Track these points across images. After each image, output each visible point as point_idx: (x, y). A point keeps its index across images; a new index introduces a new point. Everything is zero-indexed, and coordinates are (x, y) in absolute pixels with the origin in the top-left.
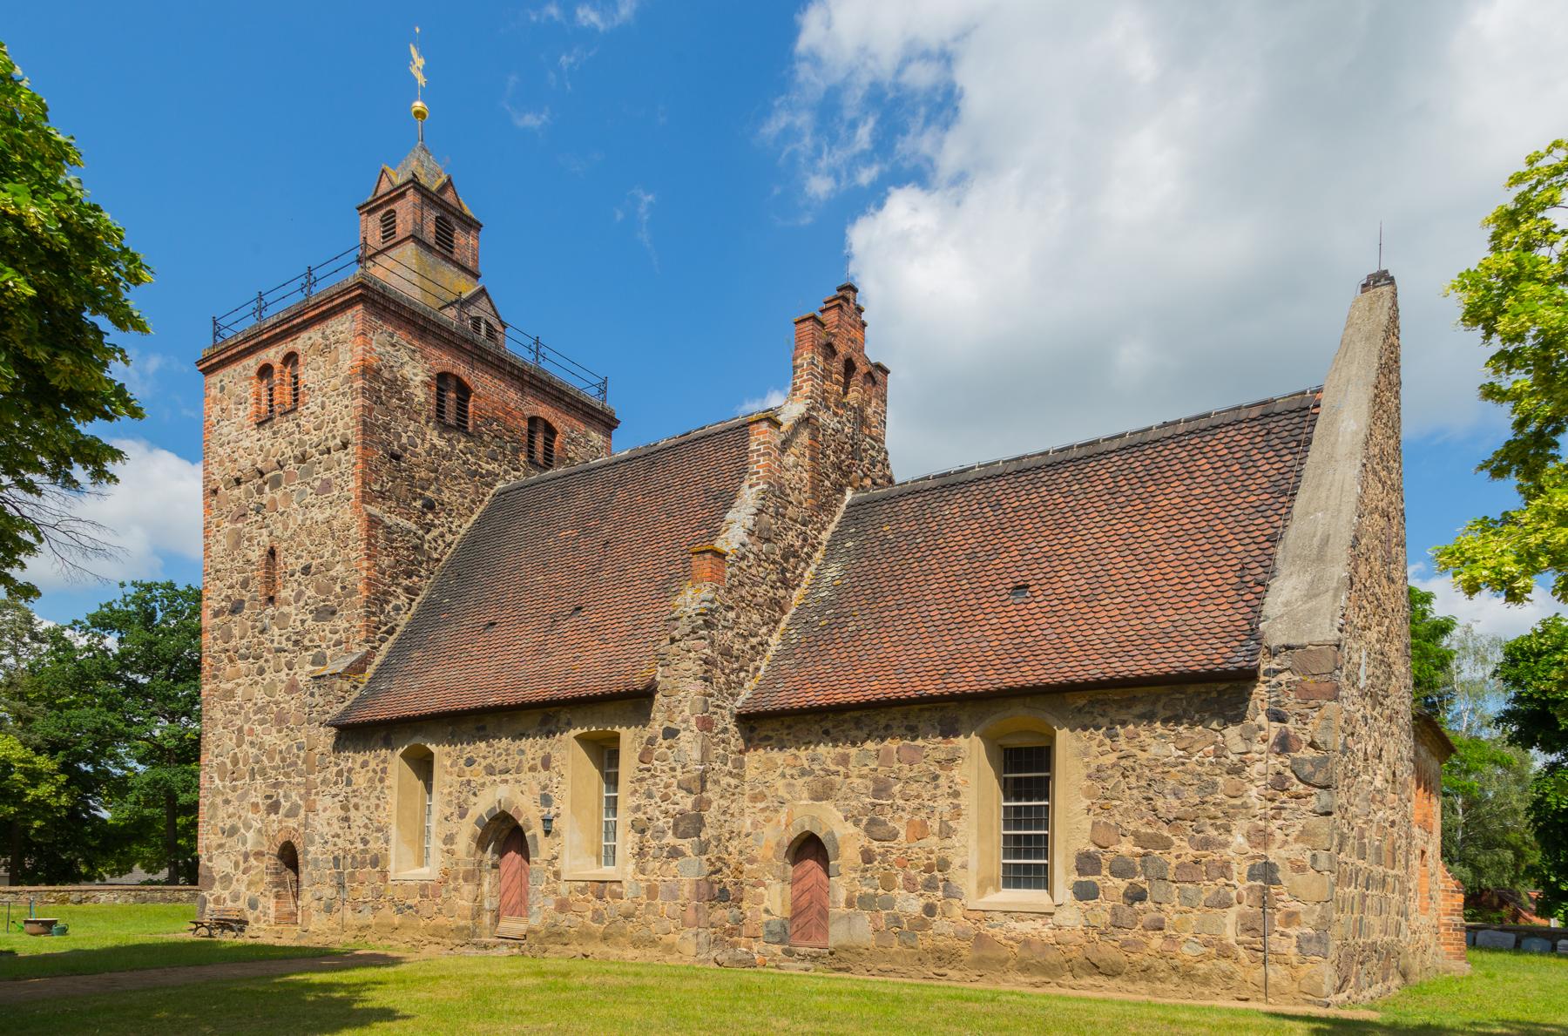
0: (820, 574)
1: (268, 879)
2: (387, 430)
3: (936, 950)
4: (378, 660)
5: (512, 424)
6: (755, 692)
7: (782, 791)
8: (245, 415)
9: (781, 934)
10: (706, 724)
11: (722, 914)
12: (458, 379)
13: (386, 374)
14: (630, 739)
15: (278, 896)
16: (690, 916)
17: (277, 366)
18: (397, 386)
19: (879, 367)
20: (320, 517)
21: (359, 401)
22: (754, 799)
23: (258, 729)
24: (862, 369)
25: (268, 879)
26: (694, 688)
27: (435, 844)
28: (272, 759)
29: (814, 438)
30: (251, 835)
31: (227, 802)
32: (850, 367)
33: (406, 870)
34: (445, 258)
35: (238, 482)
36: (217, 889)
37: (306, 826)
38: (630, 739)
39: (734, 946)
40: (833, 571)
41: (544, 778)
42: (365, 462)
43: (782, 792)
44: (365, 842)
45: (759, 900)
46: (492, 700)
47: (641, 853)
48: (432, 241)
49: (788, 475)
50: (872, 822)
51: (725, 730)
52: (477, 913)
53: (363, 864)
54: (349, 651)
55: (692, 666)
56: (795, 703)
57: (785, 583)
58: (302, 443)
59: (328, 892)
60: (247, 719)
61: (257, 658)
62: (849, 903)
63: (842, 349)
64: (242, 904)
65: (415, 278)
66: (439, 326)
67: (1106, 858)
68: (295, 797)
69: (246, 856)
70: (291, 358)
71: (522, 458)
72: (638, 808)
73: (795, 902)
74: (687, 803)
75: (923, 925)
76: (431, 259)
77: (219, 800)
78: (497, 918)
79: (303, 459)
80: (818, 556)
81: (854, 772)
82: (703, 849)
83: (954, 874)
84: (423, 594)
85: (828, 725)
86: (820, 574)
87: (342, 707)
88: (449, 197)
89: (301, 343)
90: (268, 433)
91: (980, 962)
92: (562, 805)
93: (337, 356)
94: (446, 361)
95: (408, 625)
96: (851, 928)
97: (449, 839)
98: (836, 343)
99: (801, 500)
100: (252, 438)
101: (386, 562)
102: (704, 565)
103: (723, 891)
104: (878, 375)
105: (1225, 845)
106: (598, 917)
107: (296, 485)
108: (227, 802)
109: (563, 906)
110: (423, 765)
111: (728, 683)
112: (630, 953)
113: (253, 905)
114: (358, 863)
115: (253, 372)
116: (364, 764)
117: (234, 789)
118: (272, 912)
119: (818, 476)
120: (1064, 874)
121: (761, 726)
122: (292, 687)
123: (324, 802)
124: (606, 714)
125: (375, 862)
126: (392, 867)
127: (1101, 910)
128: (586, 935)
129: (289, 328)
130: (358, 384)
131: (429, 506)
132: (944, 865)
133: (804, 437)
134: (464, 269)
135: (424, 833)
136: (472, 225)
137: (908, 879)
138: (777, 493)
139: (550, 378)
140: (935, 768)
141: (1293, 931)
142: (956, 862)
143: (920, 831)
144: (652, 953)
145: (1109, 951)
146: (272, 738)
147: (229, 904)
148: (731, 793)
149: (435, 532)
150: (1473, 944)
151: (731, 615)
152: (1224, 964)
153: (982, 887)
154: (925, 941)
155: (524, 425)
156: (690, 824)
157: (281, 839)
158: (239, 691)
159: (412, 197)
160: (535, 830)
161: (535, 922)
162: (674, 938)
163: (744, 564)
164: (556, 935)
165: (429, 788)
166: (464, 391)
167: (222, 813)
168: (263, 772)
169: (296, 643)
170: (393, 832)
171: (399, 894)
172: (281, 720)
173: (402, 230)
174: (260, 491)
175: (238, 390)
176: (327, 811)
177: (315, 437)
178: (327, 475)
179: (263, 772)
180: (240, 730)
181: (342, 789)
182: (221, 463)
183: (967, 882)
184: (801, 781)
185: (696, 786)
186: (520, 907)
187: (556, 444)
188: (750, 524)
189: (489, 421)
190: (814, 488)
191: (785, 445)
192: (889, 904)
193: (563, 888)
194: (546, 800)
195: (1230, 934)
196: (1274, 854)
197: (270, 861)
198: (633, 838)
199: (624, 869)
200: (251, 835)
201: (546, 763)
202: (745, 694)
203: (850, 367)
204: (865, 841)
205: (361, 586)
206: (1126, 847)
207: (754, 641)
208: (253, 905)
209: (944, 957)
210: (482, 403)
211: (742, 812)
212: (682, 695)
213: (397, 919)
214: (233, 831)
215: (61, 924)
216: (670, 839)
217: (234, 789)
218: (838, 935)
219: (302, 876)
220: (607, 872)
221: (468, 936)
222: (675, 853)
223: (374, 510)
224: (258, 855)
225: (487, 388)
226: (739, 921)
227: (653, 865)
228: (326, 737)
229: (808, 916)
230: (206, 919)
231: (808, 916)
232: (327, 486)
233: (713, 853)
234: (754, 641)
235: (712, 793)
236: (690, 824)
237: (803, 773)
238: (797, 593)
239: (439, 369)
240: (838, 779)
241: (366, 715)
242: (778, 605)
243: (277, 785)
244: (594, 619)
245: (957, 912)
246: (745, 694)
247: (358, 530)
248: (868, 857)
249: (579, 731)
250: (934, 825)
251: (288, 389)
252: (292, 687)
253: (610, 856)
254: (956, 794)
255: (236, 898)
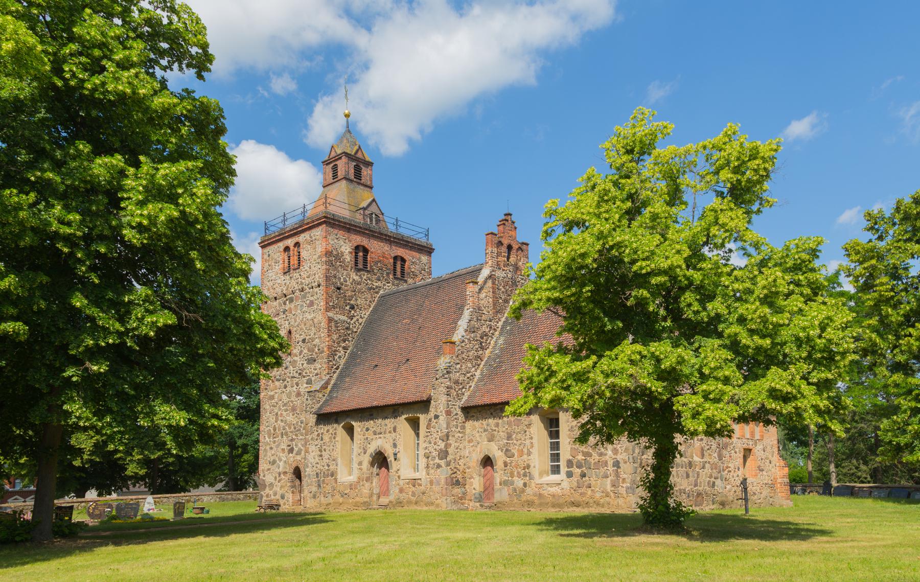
0: (497, 342)
1: (289, 484)
2: (335, 277)
3: (528, 501)
4: (332, 382)
5: (386, 261)
6: (469, 397)
7: (478, 438)
8: (278, 268)
9: (480, 499)
10: (448, 413)
11: (458, 491)
12: (364, 247)
13: (335, 253)
14: (423, 418)
15: (293, 492)
16: (444, 491)
17: (292, 248)
18: (339, 257)
19: (523, 243)
20: (309, 317)
21: (324, 267)
22: (469, 442)
23: (284, 413)
24: (515, 246)
25: (289, 484)
26: (443, 399)
27: (355, 466)
28: (290, 428)
29: (493, 283)
30: (281, 464)
31: (271, 448)
32: (510, 248)
33: (345, 477)
34: (359, 184)
35: (276, 298)
36: (267, 490)
37: (305, 459)
38: (423, 418)
39: (463, 504)
40: (502, 338)
41: (391, 435)
42: (327, 293)
43: (478, 439)
44: (328, 466)
45: (471, 484)
46: (375, 404)
47: (428, 467)
48: (352, 177)
49: (482, 302)
50: (507, 450)
51: (457, 414)
52: (371, 496)
53: (328, 476)
54: (321, 378)
55: (443, 389)
56: (480, 402)
57: (482, 348)
58: (302, 283)
59: (314, 489)
60: (280, 409)
61: (284, 380)
62: (501, 484)
63: (506, 242)
64: (278, 497)
65: (346, 206)
66: (355, 226)
67: (575, 461)
68: (300, 446)
69: (280, 474)
70: (297, 244)
71: (391, 276)
72: (426, 448)
73: (485, 484)
74: (442, 445)
75: (523, 491)
76: (352, 186)
77: (268, 448)
78: (379, 497)
79: (302, 290)
80: (497, 333)
81: (501, 430)
82: (448, 464)
83: (532, 470)
84: (350, 349)
85: (492, 411)
86: (497, 342)
87: (319, 405)
88: (359, 155)
89: (301, 238)
90: (288, 277)
91: (541, 505)
92: (400, 448)
93: (315, 245)
94: (358, 240)
95: (344, 364)
96: (501, 494)
97: (360, 463)
98: (502, 240)
99: (488, 312)
100: (282, 279)
101: (335, 337)
102: (447, 347)
103: (457, 481)
104: (524, 247)
105: (606, 455)
106: (413, 494)
107: (299, 302)
108: (271, 448)
109: (401, 491)
110: (350, 430)
111: (457, 395)
112: (425, 508)
113: (283, 497)
114: (326, 476)
115: (282, 249)
116: (328, 431)
117: (274, 442)
118: (291, 500)
119: (496, 299)
120: (564, 469)
121: (470, 411)
122: (298, 394)
123: (312, 448)
124: (414, 409)
125: (332, 475)
126: (339, 477)
127: (575, 479)
128: (409, 502)
129: (297, 231)
130: (324, 259)
131: (352, 307)
132: (528, 467)
133: (490, 283)
134: (366, 186)
135: (351, 461)
136: (369, 164)
137: (518, 473)
138: (478, 310)
139: (403, 236)
140: (525, 428)
141: (624, 485)
142: (532, 465)
143: (521, 453)
144: (432, 508)
145: (577, 497)
146: (290, 418)
147: (273, 497)
148: (460, 440)
149: (355, 319)
150: (793, 492)
151: (458, 366)
152: (607, 499)
153: (541, 474)
154: (524, 498)
155: (392, 261)
156: (444, 454)
157: (294, 466)
158: (276, 396)
159: (344, 159)
160: (391, 459)
161: (392, 498)
162: (439, 501)
163: (463, 344)
164: (400, 503)
165: (352, 439)
166: (366, 251)
167: (269, 454)
168: (286, 434)
169: (300, 374)
170: (339, 461)
171: (342, 489)
172: (294, 409)
173: (341, 174)
174: (285, 304)
175: (276, 257)
176: (313, 449)
177: (307, 281)
178: (312, 299)
179: (286, 434)
180: (277, 414)
181: (319, 442)
182: (269, 289)
183: (535, 472)
184: (484, 434)
185: (445, 438)
186: (385, 492)
187: (406, 266)
188: (465, 327)
189: (376, 263)
190: (494, 305)
191: (481, 289)
192: (512, 483)
193: (401, 483)
194: (395, 445)
195: (609, 488)
196: (619, 457)
197: (290, 476)
198: (425, 460)
199: (421, 474)
200: (281, 464)
201: (395, 430)
202: (465, 398)
203: (510, 248)
204: (504, 458)
205: (325, 349)
206: (580, 457)
207: (468, 375)
208: (283, 497)
209: (530, 504)
210: (373, 255)
211: (465, 448)
212: (440, 404)
213: (341, 500)
214: (274, 462)
215: (207, 509)
216: (437, 461)
217: (274, 442)
218: (497, 497)
219: (532, 531)
220: (417, 475)
221: (367, 505)
222: (439, 466)
223: (330, 314)
224: (285, 473)
225: (377, 248)
226: (464, 494)
227: (432, 471)
228: (312, 419)
229: (488, 489)
230: (263, 504)
231: (488, 489)
232: (312, 304)
233: (453, 465)
234: (468, 375)
235: (451, 441)
236: (444, 454)
237: (485, 431)
238: (488, 351)
239: (356, 244)
240: (496, 433)
241: (327, 410)
242: (479, 358)
243: (292, 440)
244: (413, 365)
245: (533, 485)
246: (465, 398)
247: (324, 324)
248: (506, 464)
249: (405, 416)
250: (525, 450)
251: (296, 258)
252: (298, 394)
253: (416, 469)
254: (531, 438)
255: (275, 494)
